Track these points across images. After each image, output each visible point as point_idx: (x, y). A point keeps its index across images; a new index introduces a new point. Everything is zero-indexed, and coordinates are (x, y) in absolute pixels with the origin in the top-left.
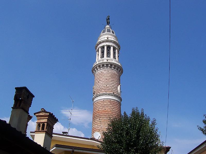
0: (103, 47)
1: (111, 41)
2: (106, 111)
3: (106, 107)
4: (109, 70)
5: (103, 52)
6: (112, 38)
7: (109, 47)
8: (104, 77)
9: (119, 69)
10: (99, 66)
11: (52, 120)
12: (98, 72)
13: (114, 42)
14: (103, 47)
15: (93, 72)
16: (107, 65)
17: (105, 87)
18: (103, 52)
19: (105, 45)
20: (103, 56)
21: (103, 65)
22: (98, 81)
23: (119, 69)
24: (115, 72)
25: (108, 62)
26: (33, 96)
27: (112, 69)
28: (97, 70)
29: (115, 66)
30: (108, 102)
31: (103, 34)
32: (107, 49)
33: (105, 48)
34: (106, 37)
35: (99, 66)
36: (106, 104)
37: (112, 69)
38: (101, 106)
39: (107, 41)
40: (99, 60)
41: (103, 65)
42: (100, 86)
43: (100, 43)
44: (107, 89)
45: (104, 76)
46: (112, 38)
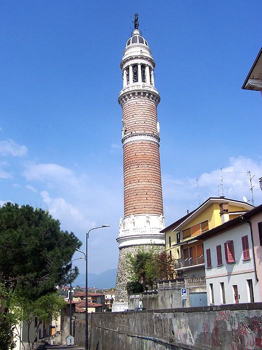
0: (135, 66)
1: (147, 58)
2: (146, 156)
3: (146, 151)
4: (146, 101)
5: (136, 74)
6: (147, 54)
7: (143, 66)
8: (138, 111)
9: (156, 99)
10: (134, 94)
11: (94, 338)
12: (131, 101)
13: (151, 61)
14: (128, 69)
15: (119, 102)
16: (145, 93)
17: (144, 124)
18: (136, 74)
19: (139, 63)
20: (136, 79)
21: (139, 93)
22: (132, 114)
23: (156, 99)
24: (152, 103)
25: (146, 90)
26: (9, 204)
27: (151, 100)
28: (126, 100)
29: (154, 96)
30: (148, 145)
31: (129, 46)
32: (133, 69)
33: (139, 67)
34: (136, 51)
35: (134, 94)
36: (146, 147)
37: (151, 100)
38: (139, 149)
39: (142, 58)
40: (129, 85)
41: (139, 93)
42: (136, 122)
43: (127, 60)
44: (146, 127)
45: (140, 109)
46: (147, 54)
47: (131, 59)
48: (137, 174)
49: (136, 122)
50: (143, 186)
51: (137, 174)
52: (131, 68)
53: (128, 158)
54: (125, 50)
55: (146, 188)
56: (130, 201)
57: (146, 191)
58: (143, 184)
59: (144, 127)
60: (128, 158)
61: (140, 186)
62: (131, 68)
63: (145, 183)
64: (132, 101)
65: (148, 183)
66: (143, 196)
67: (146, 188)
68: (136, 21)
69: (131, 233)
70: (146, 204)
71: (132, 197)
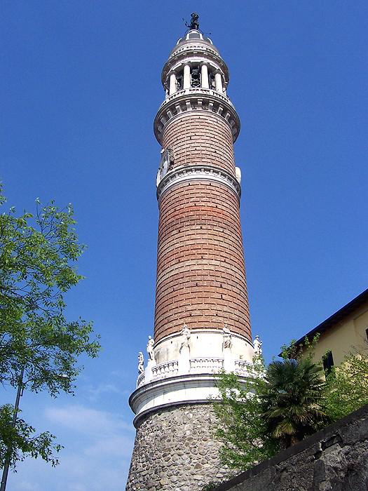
9: (235, 125)
10: (183, 104)
14: (180, 73)
33: (204, 70)
42: (198, 148)
47: (190, 54)
48: (198, 241)
49: (219, 207)
50: (212, 268)
51: (198, 241)
52: (187, 70)
53: (176, 213)
54: (174, 47)
55: (219, 274)
56: (177, 299)
57: (222, 280)
58: (210, 264)
59: (214, 158)
60: (176, 213)
61: (205, 267)
62: (187, 70)
63: (218, 263)
64: (189, 115)
65: (223, 264)
66: (213, 289)
67: (219, 274)
68: (160, 203)
69: (183, 369)
70: (219, 308)
71: (184, 291)
